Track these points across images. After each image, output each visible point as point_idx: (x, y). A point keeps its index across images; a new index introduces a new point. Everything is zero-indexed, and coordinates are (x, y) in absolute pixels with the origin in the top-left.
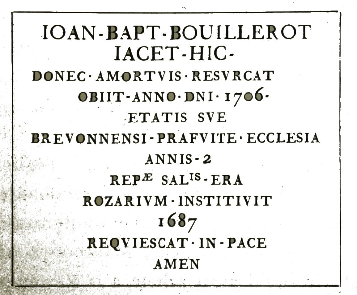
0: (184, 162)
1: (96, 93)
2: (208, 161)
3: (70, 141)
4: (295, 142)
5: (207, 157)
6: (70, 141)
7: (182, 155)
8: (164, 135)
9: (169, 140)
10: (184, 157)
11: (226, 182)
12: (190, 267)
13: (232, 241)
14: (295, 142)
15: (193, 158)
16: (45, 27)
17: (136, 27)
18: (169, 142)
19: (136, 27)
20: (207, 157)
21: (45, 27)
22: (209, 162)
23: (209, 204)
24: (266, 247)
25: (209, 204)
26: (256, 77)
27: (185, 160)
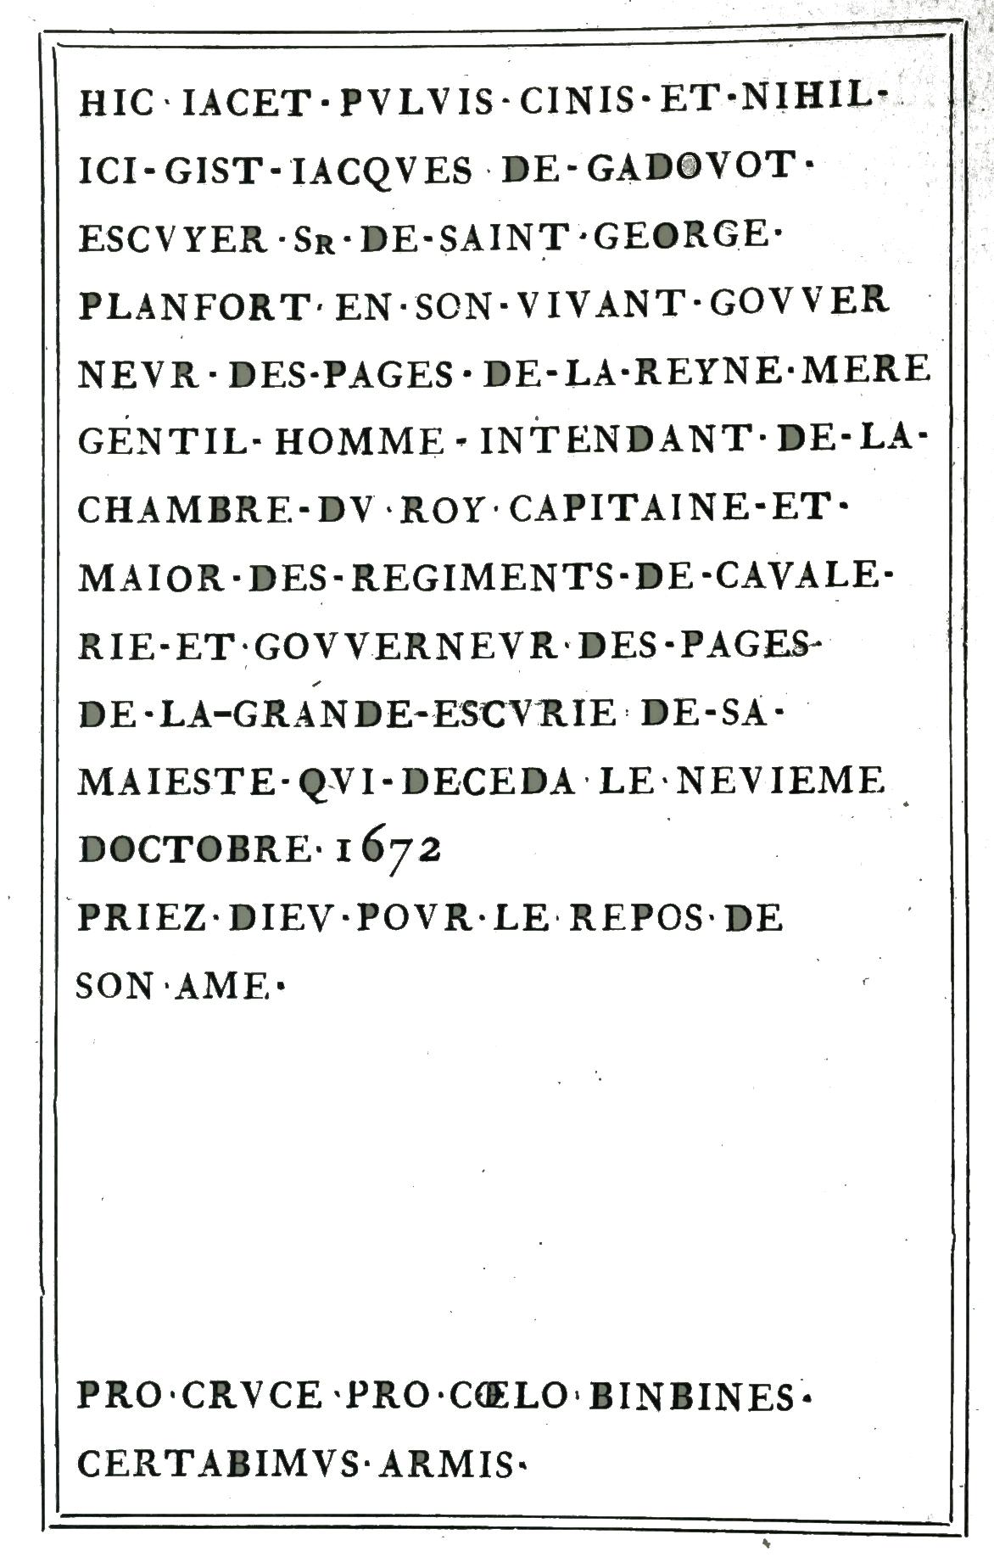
0: (208, 177)
1: (608, 1386)
2: (433, 854)
3: (253, 1400)
4: (457, 724)
5: (430, 845)
6: (253, 1400)
7: (486, 1454)
8: (96, 908)
9: (111, 923)
10: (492, 1460)
11: (420, 1470)
12: (594, 447)
13: (91, 911)
14: (457, 724)
15: (636, 97)
16: (86, 161)
17: (569, 497)
18: (111, 928)
19: (569, 497)
20: (430, 845)
21: (86, 161)
22: (436, 858)
23: (229, 790)
24: (134, 385)
25: (229, 790)
26: (601, 376)
27: (493, 1466)
